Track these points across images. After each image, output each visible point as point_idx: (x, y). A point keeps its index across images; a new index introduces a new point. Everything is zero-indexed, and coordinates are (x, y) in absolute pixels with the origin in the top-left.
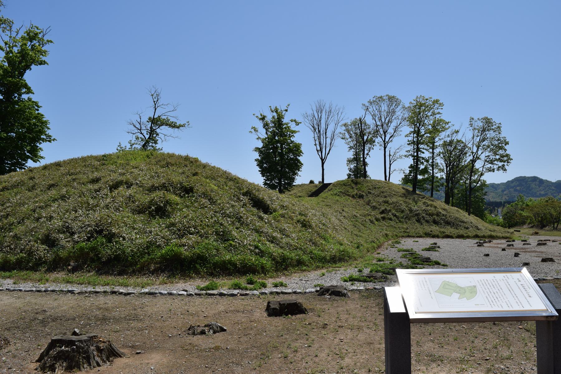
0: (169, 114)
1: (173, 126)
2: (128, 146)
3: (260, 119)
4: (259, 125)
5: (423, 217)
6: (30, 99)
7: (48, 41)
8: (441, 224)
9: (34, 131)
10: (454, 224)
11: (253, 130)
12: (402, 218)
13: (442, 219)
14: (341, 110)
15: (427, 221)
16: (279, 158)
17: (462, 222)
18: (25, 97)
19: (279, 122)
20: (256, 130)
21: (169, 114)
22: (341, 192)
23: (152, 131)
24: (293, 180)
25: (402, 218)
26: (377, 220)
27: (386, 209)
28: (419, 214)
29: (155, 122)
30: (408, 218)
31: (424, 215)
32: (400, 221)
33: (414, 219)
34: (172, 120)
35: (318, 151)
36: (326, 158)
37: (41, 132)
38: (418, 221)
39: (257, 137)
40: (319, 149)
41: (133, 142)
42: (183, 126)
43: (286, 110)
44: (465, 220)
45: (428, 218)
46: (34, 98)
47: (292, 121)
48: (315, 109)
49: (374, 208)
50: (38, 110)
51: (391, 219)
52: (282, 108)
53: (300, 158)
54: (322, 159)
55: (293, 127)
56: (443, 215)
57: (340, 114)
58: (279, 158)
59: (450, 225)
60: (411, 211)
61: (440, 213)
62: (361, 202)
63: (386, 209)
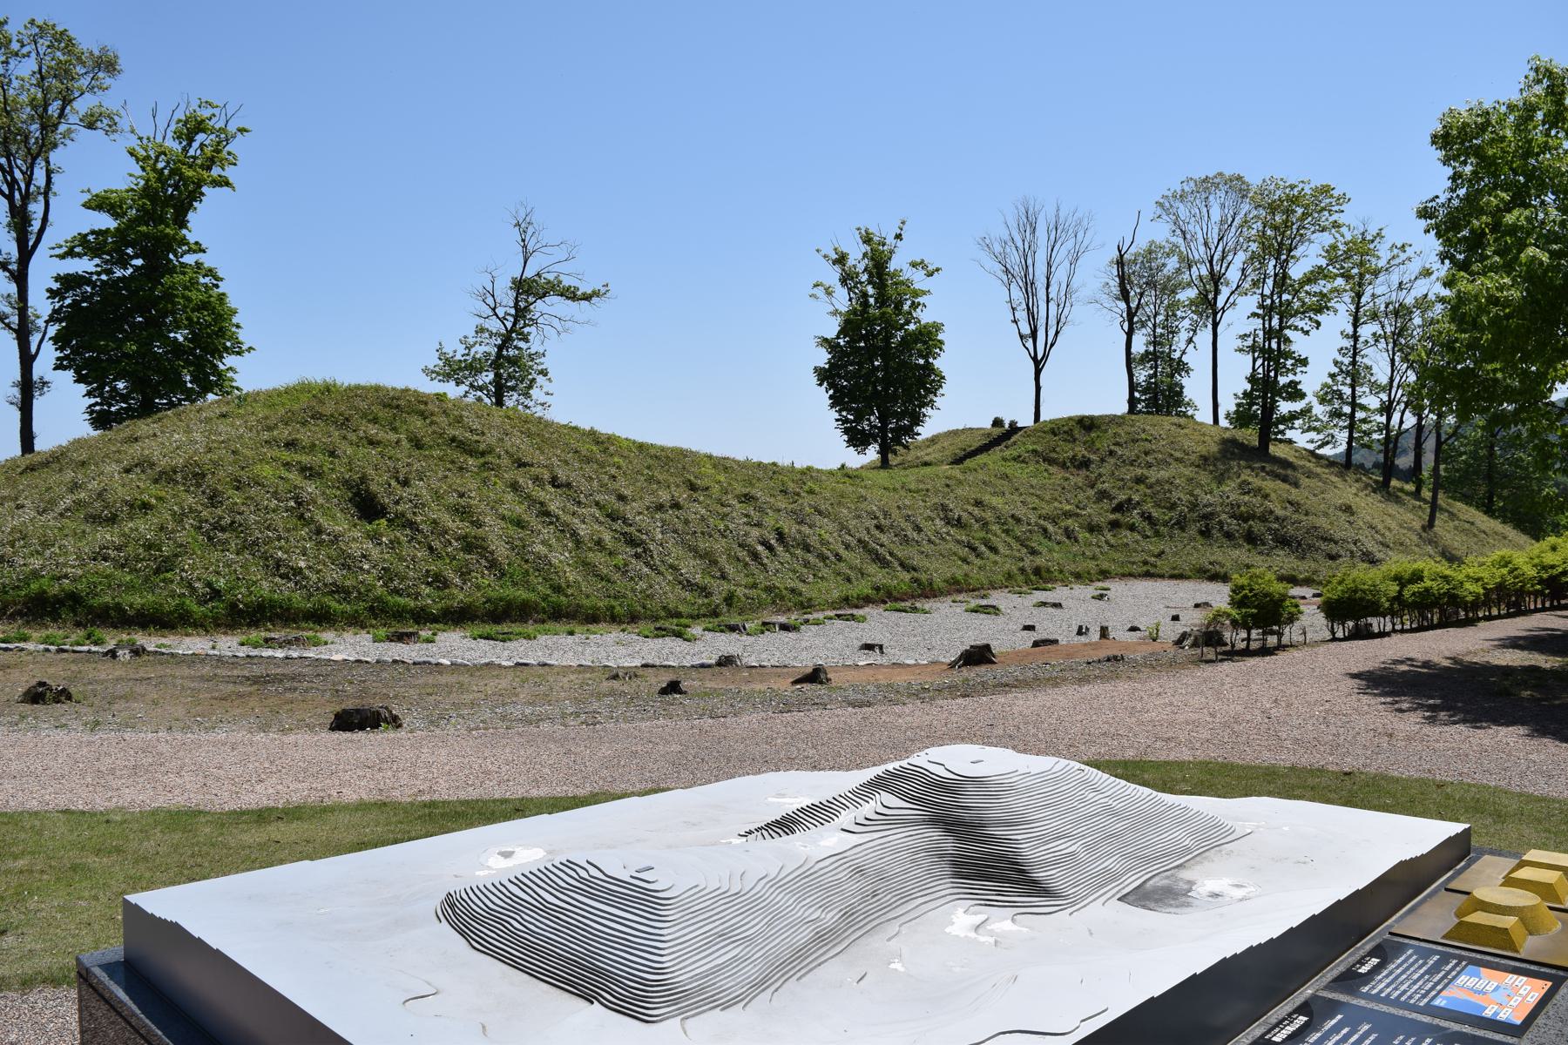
0: (557, 268)
1: (571, 295)
2: (461, 350)
3: (835, 262)
4: (832, 276)
5: (1221, 523)
6: (198, 265)
7: (242, 130)
8: (1264, 544)
9: (214, 333)
10: (1300, 544)
11: (820, 292)
12: (1165, 524)
13: (1270, 529)
14: (1085, 223)
15: (1229, 536)
16: (879, 368)
17: (1325, 539)
18: (189, 259)
19: (878, 265)
20: (829, 292)
21: (557, 268)
22: (1035, 451)
23: (521, 313)
24: (917, 419)
25: (1165, 524)
26: (1092, 529)
27: (1130, 500)
28: (1212, 514)
29: (527, 289)
30: (1181, 524)
31: (1224, 517)
32: (1157, 534)
33: (1193, 530)
34: (567, 282)
35: (1022, 337)
36: (1046, 356)
37: (222, 333)
38: (1205, 533)
39: (831, 309)
40: (1026, 330)
41: (471, 341)
42: (596, 294)
43: (898, 237)
44: (1337, 536)
45: (1233, 525)
46: (207, 260)
47: (914, 265)
48: (1013, 224)
49: (1103, 495)
50: (217, 286)
51: (1132, 528)
52: (885, 230)
53: (937, 363)
54: (1035, 359)
55: (918, 280)
56: (1277, 518)
57: (1080, 236)
58: (879, 368)
59: (1290, 545)
60: (1194, 506)
61: (1271, 512)
62: (1078, 479)
63: (1130, 500)
